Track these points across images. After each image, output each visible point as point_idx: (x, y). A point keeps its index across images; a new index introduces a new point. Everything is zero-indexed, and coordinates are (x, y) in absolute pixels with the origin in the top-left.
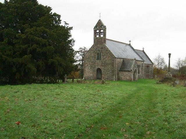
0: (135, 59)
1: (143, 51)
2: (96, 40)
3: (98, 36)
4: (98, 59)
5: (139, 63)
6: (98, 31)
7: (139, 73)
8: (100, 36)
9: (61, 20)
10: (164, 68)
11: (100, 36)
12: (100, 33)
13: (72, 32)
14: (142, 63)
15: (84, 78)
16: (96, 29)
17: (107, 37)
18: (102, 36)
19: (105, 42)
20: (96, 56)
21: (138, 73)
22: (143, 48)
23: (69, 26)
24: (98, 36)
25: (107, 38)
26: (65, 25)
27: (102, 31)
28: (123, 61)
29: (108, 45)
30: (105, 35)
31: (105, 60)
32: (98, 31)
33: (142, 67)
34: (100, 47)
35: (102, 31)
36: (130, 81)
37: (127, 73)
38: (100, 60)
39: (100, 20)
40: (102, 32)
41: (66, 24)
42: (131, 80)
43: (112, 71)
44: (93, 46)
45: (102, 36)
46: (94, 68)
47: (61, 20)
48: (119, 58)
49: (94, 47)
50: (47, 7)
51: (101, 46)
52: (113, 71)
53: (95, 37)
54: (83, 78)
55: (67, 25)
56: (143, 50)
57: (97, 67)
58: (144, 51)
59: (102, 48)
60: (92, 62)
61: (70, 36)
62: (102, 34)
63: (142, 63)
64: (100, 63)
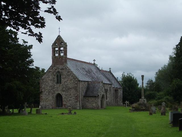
0: (102, 82)
1: (110, 72)
2: (54, 59)
3: (57, 55)
4: (58, 83)
5: (107, 87)
6: (57, 49)
7: (107, 99)
8: (59, 54)
9: (19, 38)
10: (176, 55)
11: (59, 54)
12: (60, 50)
13: (32, 51)
14: (110, 86)
15: (40, 107)
16: (55, 46)
17: (69, 56)
18: (62, 54)
19: (66, 62)
20: (56, 79)
21: (106, 99)
22: (94, 60)
23: (28, 44)
24: (57, 55)
25: (68, 57)
26: (24, 44)
27: (62, 49)
28: (88, 84)
29: (69, 65)
30: (66, 54)
31: (66, 84)
32: (57, 49)
33: (110, 91)
34: (60, 68)
35: (62, 49)
36: (97, 108)
37: (93, 99)
38: (60, 83)
39: (59, 36)
40: (62, 50)
41: (25, 42)
42: (99, 107)
43: (76, 96)
44: (52, 67)
45: (62, 54)
46: (53, 94)
47: (19, 38)
48: (83, 81)
49: (52, 68)
50: (126, 76)
51: (61, 67)
52: (77, 98)
53: (54, 56)
54: (39, 107)
55: (26, 44)
56: (110, 71)
57: (57, 92)
58: (112, 72)
59: (62, 69)
60: (51, 86)
61: (30, 56)
62: (62, 53)
63: (110, 86)
64: (61, 88)
